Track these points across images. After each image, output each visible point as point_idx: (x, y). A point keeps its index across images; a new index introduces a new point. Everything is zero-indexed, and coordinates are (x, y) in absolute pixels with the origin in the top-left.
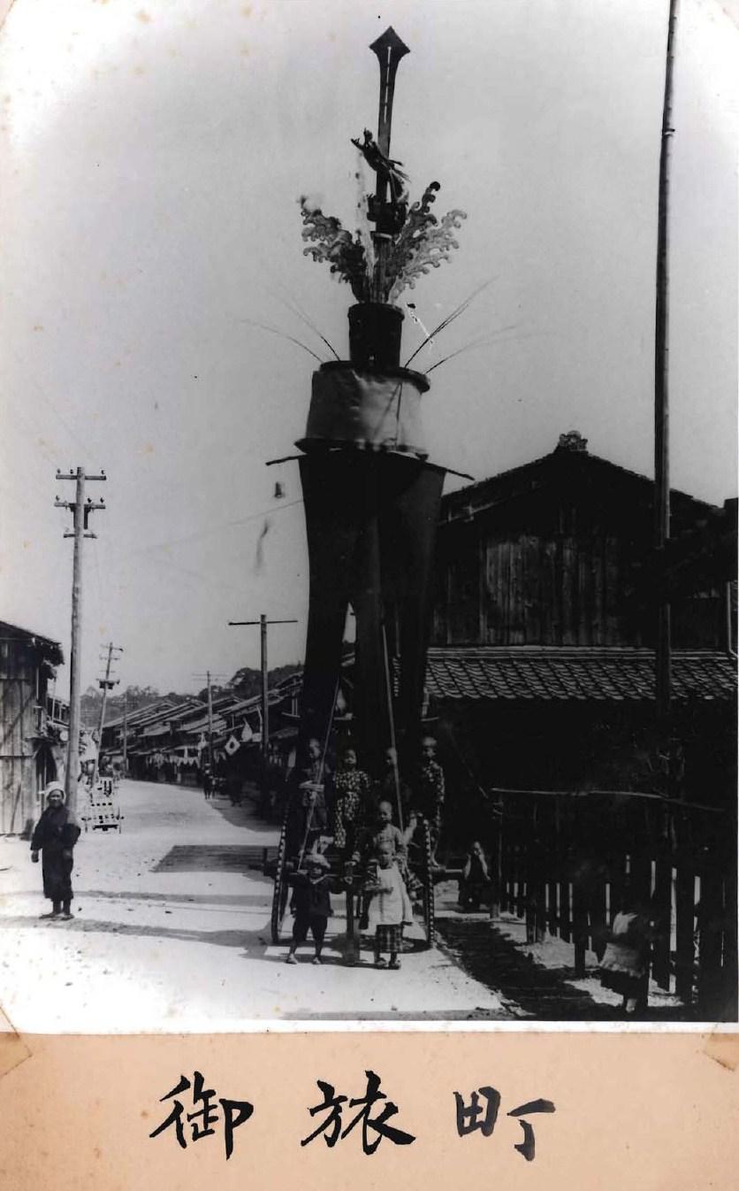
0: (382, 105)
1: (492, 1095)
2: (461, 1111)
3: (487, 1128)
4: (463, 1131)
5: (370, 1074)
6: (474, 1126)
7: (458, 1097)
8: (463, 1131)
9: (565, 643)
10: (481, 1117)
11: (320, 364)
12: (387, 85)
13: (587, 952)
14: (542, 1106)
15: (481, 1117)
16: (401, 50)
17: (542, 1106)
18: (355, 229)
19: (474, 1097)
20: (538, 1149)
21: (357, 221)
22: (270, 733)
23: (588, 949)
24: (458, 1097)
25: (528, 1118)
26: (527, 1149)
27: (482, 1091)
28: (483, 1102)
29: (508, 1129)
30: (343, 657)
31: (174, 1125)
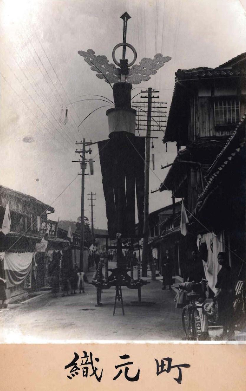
0: (124, 32)
1: (169, 360)
2: (158, 366)
3: (168, 371)
4: (158, 373)
5: (76, 354)
6: (162, 371)
7: (157, 361)
8: (158, 373)
9: (206, 99)
10: (166, 368)
11: (161, 53)
12: (125, 27)
13: (206, 292)
14: (186, 366)
15: (166, 368)
16: (129, 17)
17: (186, 366)
18: (75, 376)
19: (163, 362)
20: (182, 381)
21: (160, 186)
22: (239, 109)
23: (207, 291)
24: (157, 361)
25: (181, 368)
26: (179, 380)
27: (165, 359)
28: (166, 362)
29: (175, 372)
30: (90, 228)
31: (127, 47)
